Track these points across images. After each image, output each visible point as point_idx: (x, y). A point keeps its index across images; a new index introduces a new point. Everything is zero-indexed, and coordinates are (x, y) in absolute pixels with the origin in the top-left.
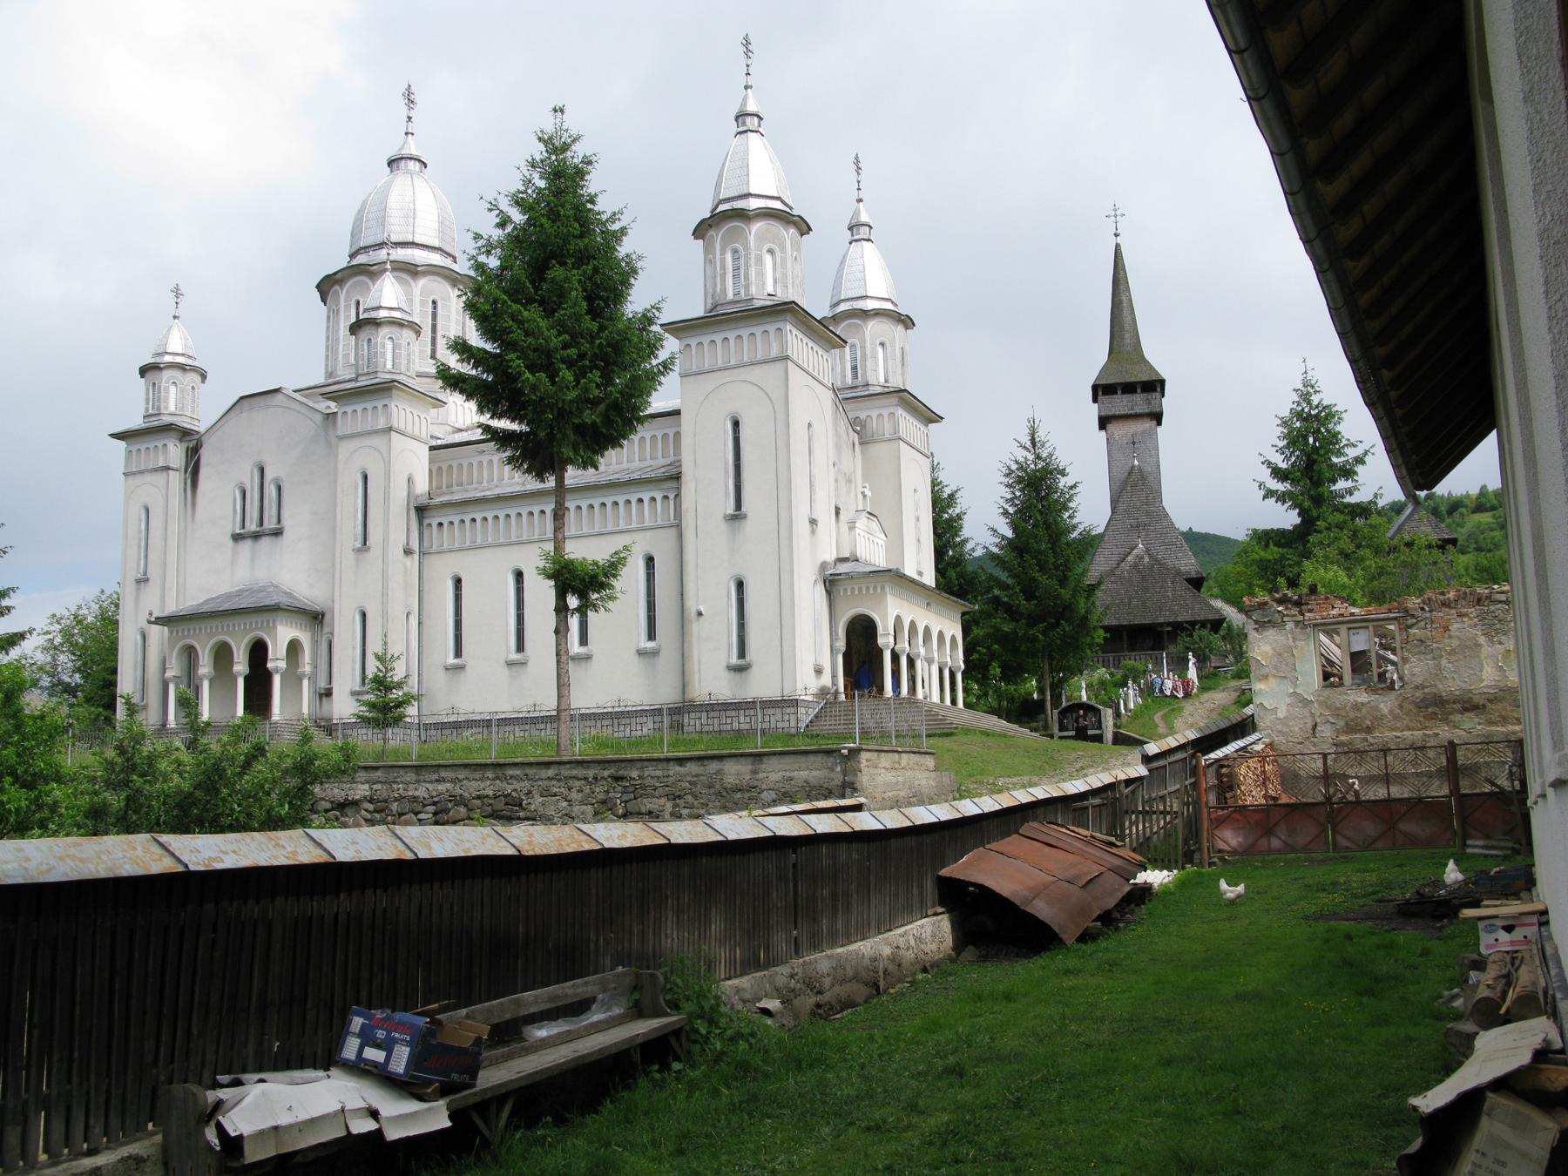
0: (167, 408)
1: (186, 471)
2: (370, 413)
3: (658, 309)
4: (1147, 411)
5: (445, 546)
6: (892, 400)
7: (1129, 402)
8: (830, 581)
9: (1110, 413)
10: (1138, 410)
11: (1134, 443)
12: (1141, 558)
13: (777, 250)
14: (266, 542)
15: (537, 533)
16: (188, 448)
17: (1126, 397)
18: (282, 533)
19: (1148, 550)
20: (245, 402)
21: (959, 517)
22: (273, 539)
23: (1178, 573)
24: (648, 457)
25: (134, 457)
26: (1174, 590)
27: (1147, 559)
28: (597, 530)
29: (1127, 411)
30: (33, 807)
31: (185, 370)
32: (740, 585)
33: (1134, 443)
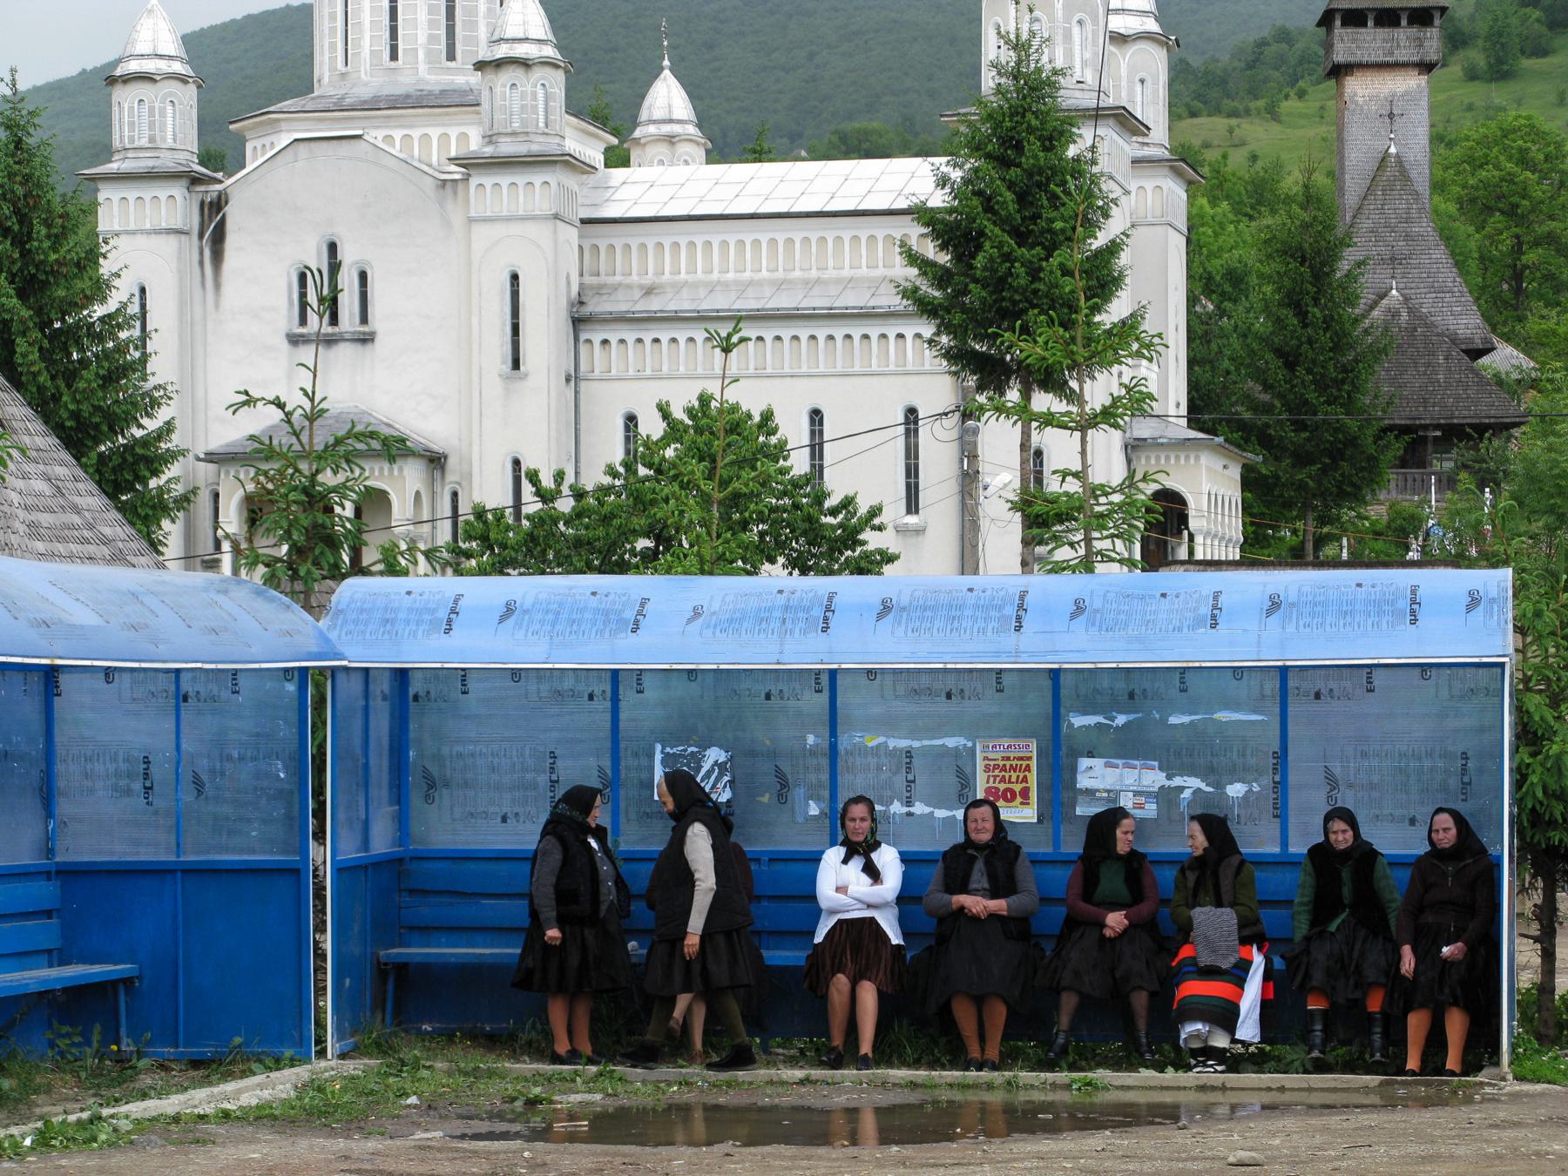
0: (164, 139)
1: (201, 236)
2: (505, 191)
3: (1128, 236)
4: (1416, 59)
5: (614, 372)
6: (1070, 102)
7: (1385, 41)
8: (1133, 447)
9: (1352, 59)
10: (1402, 56)
11: (1391, 116)
12: (1395, 314)
13: (1088, 22)
14: (344, 351)
15: (752, 366)
16: (202, 204)
17: (1383, 32)
18: (372, 340)
19: (1406, 299)
20: (302, 147)
21: (1113, 248)
22: (359, 346)
23: (1454, 340)
24: (881, 264)
25: (116, 209)
26: (1449, 369)
27: (1404, 316)
28: (839, 369)
29: (1381, 59)
30: (1521, 687)
31: (154, 81)
32: (515, 278)
33: (1391, 116)
